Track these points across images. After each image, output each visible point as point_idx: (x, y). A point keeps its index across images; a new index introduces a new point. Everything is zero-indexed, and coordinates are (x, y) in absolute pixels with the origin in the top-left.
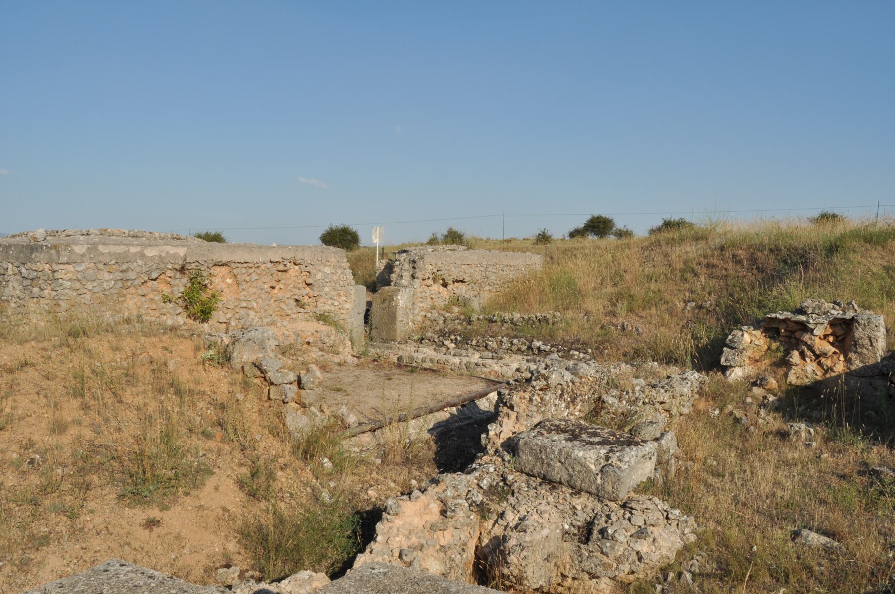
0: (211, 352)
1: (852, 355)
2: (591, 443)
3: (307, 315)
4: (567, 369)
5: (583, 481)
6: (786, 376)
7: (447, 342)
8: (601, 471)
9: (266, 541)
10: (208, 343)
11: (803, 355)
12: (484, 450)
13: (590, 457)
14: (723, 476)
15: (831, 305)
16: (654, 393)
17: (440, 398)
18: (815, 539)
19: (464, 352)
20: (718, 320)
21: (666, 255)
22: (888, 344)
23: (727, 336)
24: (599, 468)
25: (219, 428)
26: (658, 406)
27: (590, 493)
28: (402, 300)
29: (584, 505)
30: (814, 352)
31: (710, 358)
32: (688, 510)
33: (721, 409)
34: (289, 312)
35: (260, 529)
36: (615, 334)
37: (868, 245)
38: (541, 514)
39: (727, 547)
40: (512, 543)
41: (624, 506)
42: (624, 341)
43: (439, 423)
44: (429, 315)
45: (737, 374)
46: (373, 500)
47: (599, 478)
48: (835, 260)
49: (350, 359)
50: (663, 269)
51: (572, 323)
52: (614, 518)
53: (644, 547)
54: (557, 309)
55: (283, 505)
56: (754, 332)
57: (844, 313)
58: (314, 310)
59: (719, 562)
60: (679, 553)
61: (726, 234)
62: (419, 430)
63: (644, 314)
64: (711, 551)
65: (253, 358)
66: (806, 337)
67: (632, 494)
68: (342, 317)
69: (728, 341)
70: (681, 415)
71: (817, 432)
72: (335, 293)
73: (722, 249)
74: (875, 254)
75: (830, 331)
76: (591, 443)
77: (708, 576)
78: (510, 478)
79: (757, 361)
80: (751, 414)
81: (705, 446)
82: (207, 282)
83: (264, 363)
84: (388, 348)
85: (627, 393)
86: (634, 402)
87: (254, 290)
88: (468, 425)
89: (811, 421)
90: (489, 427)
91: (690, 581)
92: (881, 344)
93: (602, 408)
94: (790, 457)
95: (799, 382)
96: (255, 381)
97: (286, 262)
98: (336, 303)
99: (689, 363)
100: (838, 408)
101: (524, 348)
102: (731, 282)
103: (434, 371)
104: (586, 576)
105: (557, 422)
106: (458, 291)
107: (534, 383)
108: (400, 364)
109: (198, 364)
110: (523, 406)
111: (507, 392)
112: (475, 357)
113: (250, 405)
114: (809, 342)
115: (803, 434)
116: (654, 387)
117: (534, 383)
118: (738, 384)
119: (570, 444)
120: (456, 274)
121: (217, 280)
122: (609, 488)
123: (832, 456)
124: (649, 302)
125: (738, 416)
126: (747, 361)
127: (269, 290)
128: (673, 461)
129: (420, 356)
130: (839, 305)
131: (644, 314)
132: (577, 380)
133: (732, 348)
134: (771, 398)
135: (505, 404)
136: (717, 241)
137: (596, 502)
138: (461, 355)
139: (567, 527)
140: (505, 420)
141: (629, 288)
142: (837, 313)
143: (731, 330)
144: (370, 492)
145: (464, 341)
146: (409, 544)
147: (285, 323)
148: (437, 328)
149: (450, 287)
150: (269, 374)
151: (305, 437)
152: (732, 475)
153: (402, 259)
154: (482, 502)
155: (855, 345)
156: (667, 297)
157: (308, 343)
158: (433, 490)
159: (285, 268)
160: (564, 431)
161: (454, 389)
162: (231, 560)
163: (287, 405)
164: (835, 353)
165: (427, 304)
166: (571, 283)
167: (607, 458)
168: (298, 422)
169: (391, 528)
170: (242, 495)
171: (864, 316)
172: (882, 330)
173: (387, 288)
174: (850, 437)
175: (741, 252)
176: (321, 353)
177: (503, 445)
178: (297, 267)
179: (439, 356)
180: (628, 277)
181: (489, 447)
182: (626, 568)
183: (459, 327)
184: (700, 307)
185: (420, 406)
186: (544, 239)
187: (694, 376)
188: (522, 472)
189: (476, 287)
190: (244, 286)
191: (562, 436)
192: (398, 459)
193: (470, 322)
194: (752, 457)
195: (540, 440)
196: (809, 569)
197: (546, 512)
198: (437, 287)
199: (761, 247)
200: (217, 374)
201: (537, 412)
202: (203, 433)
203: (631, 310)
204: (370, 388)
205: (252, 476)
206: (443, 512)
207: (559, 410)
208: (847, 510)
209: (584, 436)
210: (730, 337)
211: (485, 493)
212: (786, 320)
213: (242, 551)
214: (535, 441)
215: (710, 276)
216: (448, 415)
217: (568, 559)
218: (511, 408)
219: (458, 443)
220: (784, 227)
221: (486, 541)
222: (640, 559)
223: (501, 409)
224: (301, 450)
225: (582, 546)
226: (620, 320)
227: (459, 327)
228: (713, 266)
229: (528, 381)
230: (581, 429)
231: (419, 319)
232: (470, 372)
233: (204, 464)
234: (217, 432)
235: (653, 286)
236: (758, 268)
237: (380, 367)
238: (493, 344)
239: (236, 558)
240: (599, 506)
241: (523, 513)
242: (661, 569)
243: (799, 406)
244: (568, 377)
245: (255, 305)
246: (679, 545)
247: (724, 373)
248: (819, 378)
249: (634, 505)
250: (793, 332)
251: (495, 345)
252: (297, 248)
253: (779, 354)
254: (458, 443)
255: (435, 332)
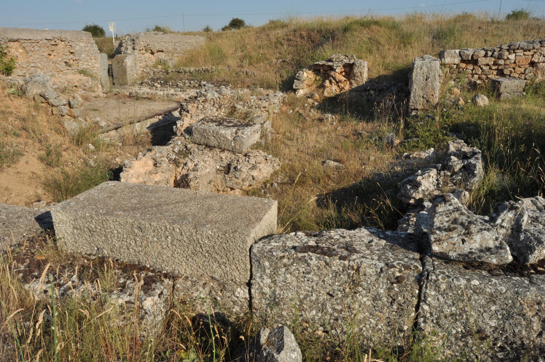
0: (13, 90)
1: (353, 81)
2: (229, 126)
3: (73, 71)
4: (216, 91)
5: (225, 145)
6: (323, 92)
7: (156, 84)
8: (234, 139)
9: (60, 187)
10: (10, 84)
11: (331, 82)
12: (175, 134)
13: (228, 133)
14: (293, 140)
15: (344, 57)
16: (260, 102)
17: (153, 111)
18: (332, 164)
19: (165, 89)
20: (292, 67)
21: (268, 35)
22: (369, 75)
23: (296, 74)
24: (233, 138)
25: (25, 131)
26: (262, 109)
27: (229, 151)
28: (129, 62)
29: (226, 156)
30: (335, 80)
31: (288, 86)
32: (276, 155)
33: (293, 110)
34: (62, 69)
35: (55, 181)
36: (243, 76)
37: (362, 27)
38: (205, 162)
39: (293, 170)
40: (191, 176)
41: (245, 155)
42: (247, 80)
43: (153, 124)
44: (145, 70)
45: (301, 93)
46: (119, 163)
47: (233, 143)
48: (347, 35)
49: (101, 95)
50: (266, 42)
51: (221, 71)
52: (241, 161)
53: (255, 173)
54: (213, 65)
55: (68, 169)
56: (309, 72)
57: (350, 61)
58: (77, 68)
59: (290, 177)
60: (272, 175)
61: (297, 24)
62: (142, 128)
63: (257, 66)
64: (287, 173)
65: (39, 92)
66: (332, 73)
67: (249, 150)
68: (94, 71)
69: (296, 77)
70: (274, 113)
71: (336, 118)
72: (89, 58)
73: (295, 31)
74: (365, 32)
75: (343, 70)
76: (229, 126)
77: (284, 184)
78: (189, 146)
79: (310, 86)
80: (307, 111)
81: (285, 126)
82: (6, 51)
83: (46, 94)
84: (123, 89)
85: (247, 103)
86: (251, 107)
87: (38, 56)
88: (168, 124)
89: (333, 113)
90: (177, 122)
91: (277, 186)
92: (365, 75)
93: (235, 111)
94: (323, 129)
95: (329, 96)
96: (42, 105)
97: (56, 40)
98: (90, 64)
99: (278, 89)
100: (346, 106)
101: (197, 85)
102: (299, 48)
103: (149, 99)
104: (229, 190)
105: (212, 118)
106: (160, 57)
107: (199, 99)
108: (130, 96)
109: (5, 96)
110: (194, 111)
111: (185, 104)
112: (172, 91)
113: (42, 119)
114: (334, 76)
115: (330, 119)
116: (260, 99)
117: (199, 99)
118: (301, 98)
119: (218, 127)
120: (158, 47)
121: (13, 50)
122: (238, 147)
123: (342, 128)
124: (259, 59)
125: (301, 112)
126: (305, 86)
127: (47, 56)
128: (270, 135)
129: (142, 92)
130: (347, 57)
131: (257, 66)
132: (221, 97)
133: (298, 80)
134: (316, 103)
135: (184, 110)
136: (293, 27)
137: (232, 154)
138: (164, 90)
139: (218, 167)
140: (185, 118)
141: (249, 53)
142: (346, 61)
143: (298, 71)
144: (117, 159)
145: (165, 83)
146: (139, 181)
147: (60, 75)
148: (150, 77)
149: (156, 54)
150: (50, 100)
151: (77, 134)
152: (297, 139)
153: (126, 39)
154: (175, 159)
155: (354, 76)
156: (268, 56)
157: (76, 86)
158: (149, 154)
159: (56, 43)
160: (215, 122)
161: (160, 107)
162: (41, 198)
163: (64, 117)
164: (345, 80)
165: (143, 64)
166: (220, 51)
167: (236, 133)
168: (71, 125)
169: (128, 175)
170: (43, 165)
171: (358, 62)
172: (366, 69)
173: (119, 55)
174: (350, 119)
175: (304, 32)
176: (84, 92)
177: (185, 131)
178: (63, 43)
179: (153, 91)
180: (248, 47)
181: (177, 132)
182: (247, 183)
183: (162, 76)
184: (284, 61)
185: (141, 116)
186: (207, 30)
187: (280, 94)
188: (195, 143)
189: (170, 54)
190: (31, 54)
191: (214, 124)
192: (131, 142)
193: (167, 73)
194: (306, 131)
195: (203, 127)
196: (329, 177)
197: (207, 161)
198: (148, 55)
199: (313, 30)
200: (18, 102)
201: (201, 113)
202: (14, 134)
203: (250, 64)
204: (114, 108)
205: (48, 155)
206: (155, 165)
207: (213, 112)
208: (346, 151)
209: (225, 123)
210: (297, 74)
211: (176, 154)
212: (323, 65)
213: (47, 193)
214: (201, 127)
215: (289, 45)
216: (157, 120)
217: (220, 182)
218: (188, 112)
219: (162, 133)
220: (325, 20)
221: (179, 178)
222: (254, 179)
223: (182, 113)
224: (75, 141)
225: (226, 175)
226: (245, 69)
227: (162, 76)
228: (291, 40)
229: (196, 98)
230: (224, 120)
231: (140, 72)
232: (169, 98)
233: (17, 151)
234: (23, 133)
235: (261, 51)
236: (311, 41)
237: (119, 98)
238: (180, 84)
239: (43, 197)
240: (233, 156)
241: (196, 162)
242: (264, 183)
243: (329, 106)
244: (217, 95)
245: (40, 65)
246: (272, 171)
247: (295, 93)
248: (338, 93)
249: (250, 154)
250: (326, 71)
251: (182, 85)
252: (61, 32)
253: (320, 82)
254: (162, 133)
255: (149, 79)
